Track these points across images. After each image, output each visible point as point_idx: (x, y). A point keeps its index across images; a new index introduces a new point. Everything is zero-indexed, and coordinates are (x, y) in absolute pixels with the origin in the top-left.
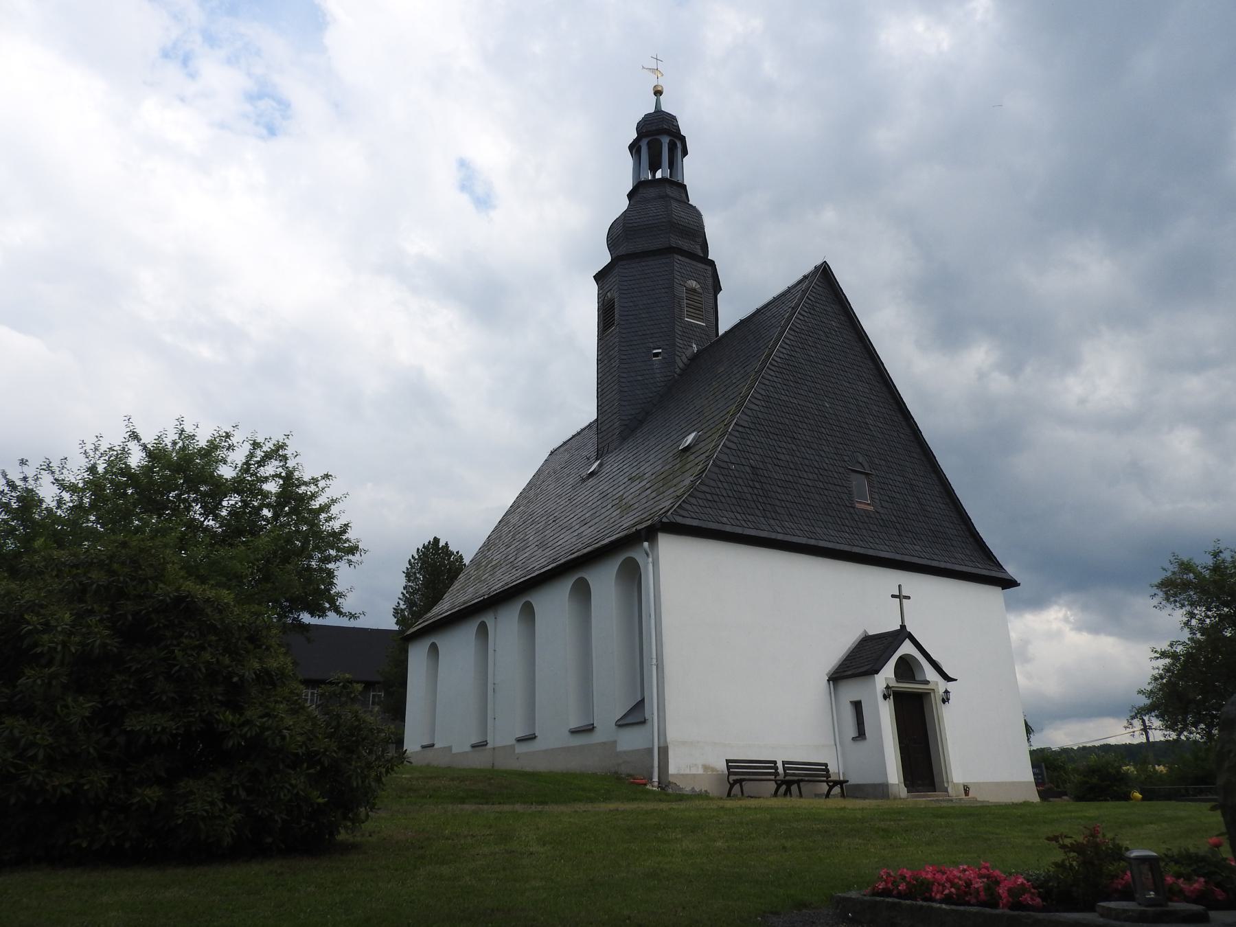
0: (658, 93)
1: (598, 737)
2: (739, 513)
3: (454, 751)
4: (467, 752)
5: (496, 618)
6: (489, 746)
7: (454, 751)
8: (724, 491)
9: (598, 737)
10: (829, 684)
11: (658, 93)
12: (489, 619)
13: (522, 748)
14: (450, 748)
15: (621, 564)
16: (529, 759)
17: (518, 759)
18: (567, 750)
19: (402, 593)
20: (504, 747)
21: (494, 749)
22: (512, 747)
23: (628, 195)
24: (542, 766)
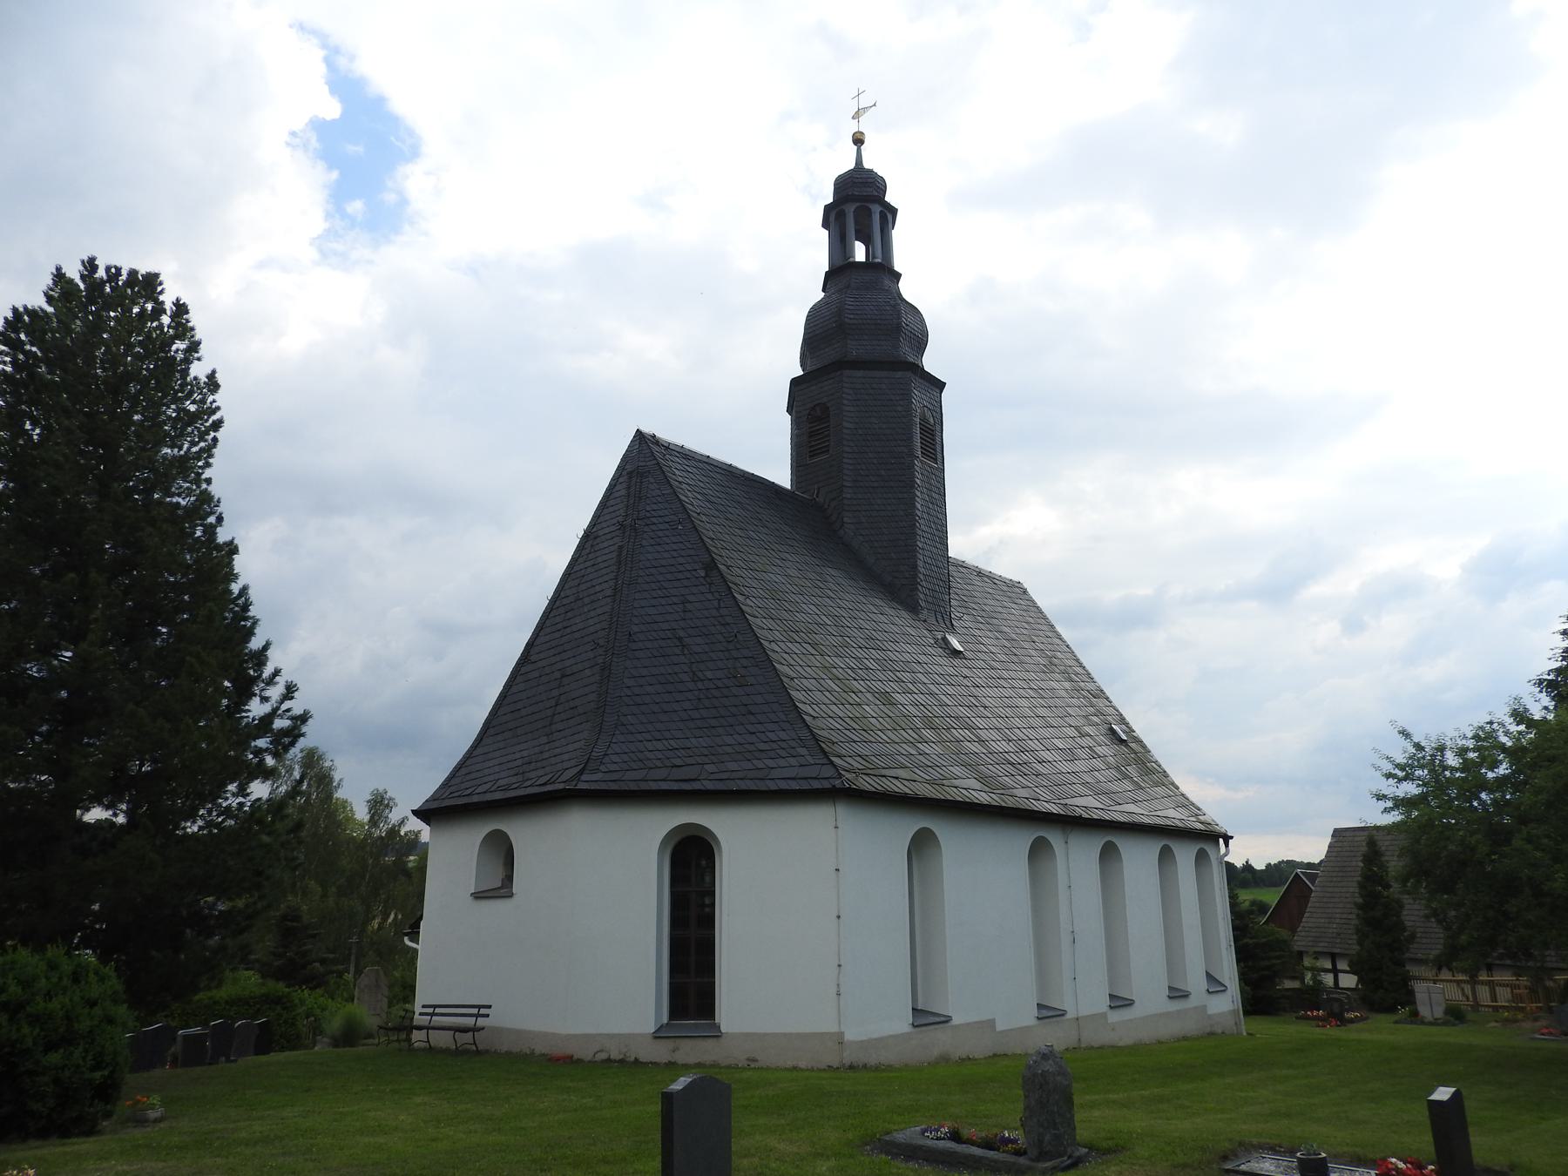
0: (858, 140)
1: (1192, 1002)
2: (783, 749)
3: (1000, 1027)
4: (1028, 1028)
5: (1066, 842)
6: (1068, 1016)
7: (1000, 1027)
8: (581, 586)
9: (1192, 1002)
10: (1352, 1021)
11: (858, 140)
12: (1055, 838)
13: (1116, 1017)
14: (991, 1023)
15: (487, 835)
16: (1123, 1028)
17: (1113, 1029)
18: (1167, 1015)
19: (249, 711)
20: (1093, 1016)
21: (1077, 1019)
22: (1104, 1015)
23: (825, 206)
24: (1146, 1034)
